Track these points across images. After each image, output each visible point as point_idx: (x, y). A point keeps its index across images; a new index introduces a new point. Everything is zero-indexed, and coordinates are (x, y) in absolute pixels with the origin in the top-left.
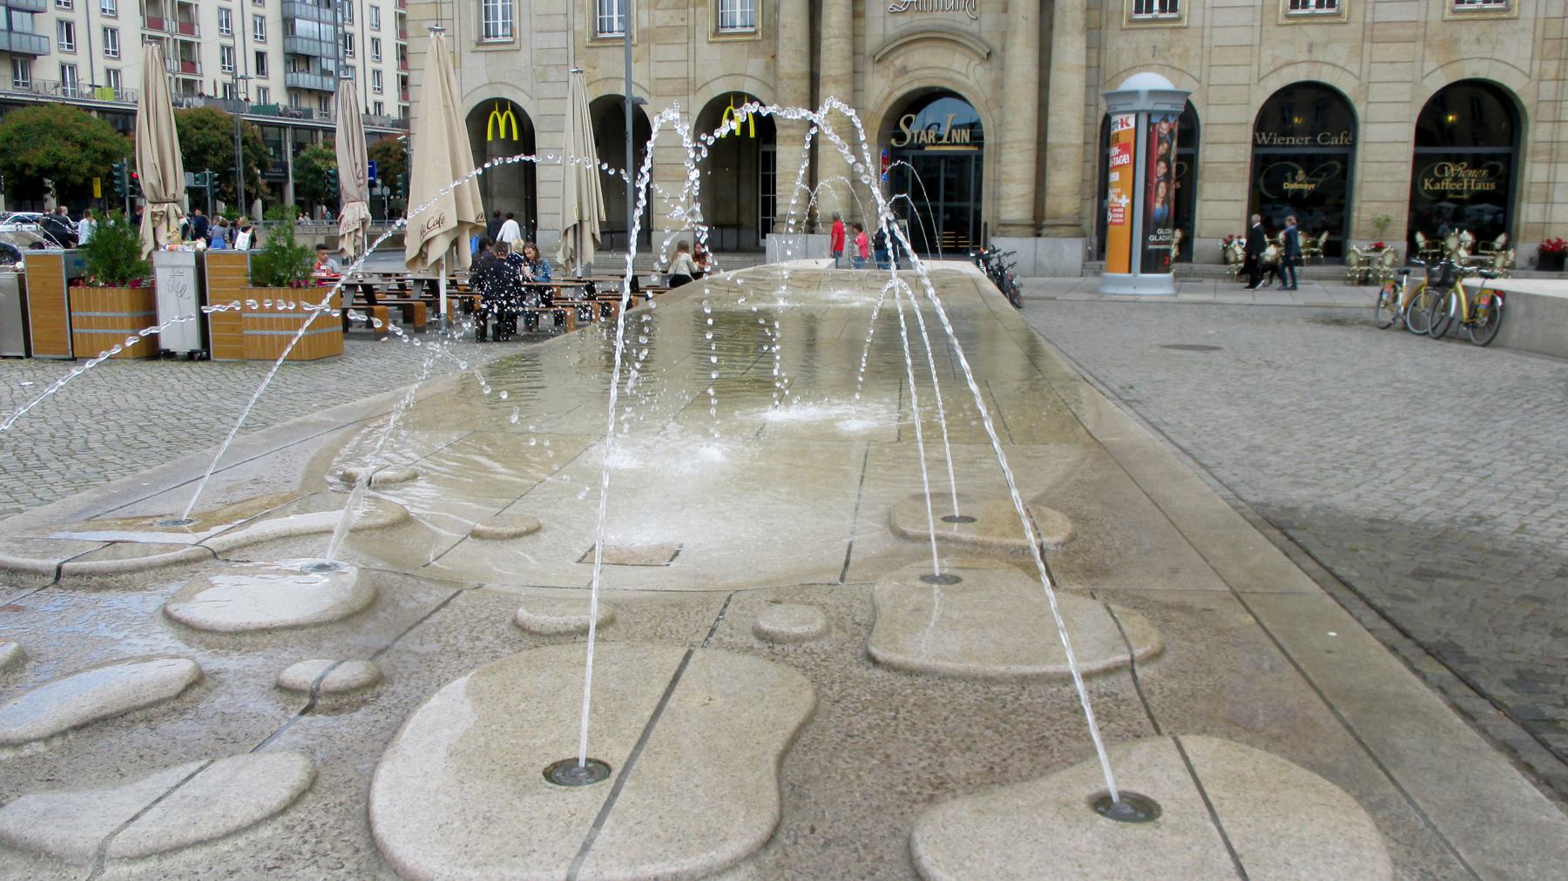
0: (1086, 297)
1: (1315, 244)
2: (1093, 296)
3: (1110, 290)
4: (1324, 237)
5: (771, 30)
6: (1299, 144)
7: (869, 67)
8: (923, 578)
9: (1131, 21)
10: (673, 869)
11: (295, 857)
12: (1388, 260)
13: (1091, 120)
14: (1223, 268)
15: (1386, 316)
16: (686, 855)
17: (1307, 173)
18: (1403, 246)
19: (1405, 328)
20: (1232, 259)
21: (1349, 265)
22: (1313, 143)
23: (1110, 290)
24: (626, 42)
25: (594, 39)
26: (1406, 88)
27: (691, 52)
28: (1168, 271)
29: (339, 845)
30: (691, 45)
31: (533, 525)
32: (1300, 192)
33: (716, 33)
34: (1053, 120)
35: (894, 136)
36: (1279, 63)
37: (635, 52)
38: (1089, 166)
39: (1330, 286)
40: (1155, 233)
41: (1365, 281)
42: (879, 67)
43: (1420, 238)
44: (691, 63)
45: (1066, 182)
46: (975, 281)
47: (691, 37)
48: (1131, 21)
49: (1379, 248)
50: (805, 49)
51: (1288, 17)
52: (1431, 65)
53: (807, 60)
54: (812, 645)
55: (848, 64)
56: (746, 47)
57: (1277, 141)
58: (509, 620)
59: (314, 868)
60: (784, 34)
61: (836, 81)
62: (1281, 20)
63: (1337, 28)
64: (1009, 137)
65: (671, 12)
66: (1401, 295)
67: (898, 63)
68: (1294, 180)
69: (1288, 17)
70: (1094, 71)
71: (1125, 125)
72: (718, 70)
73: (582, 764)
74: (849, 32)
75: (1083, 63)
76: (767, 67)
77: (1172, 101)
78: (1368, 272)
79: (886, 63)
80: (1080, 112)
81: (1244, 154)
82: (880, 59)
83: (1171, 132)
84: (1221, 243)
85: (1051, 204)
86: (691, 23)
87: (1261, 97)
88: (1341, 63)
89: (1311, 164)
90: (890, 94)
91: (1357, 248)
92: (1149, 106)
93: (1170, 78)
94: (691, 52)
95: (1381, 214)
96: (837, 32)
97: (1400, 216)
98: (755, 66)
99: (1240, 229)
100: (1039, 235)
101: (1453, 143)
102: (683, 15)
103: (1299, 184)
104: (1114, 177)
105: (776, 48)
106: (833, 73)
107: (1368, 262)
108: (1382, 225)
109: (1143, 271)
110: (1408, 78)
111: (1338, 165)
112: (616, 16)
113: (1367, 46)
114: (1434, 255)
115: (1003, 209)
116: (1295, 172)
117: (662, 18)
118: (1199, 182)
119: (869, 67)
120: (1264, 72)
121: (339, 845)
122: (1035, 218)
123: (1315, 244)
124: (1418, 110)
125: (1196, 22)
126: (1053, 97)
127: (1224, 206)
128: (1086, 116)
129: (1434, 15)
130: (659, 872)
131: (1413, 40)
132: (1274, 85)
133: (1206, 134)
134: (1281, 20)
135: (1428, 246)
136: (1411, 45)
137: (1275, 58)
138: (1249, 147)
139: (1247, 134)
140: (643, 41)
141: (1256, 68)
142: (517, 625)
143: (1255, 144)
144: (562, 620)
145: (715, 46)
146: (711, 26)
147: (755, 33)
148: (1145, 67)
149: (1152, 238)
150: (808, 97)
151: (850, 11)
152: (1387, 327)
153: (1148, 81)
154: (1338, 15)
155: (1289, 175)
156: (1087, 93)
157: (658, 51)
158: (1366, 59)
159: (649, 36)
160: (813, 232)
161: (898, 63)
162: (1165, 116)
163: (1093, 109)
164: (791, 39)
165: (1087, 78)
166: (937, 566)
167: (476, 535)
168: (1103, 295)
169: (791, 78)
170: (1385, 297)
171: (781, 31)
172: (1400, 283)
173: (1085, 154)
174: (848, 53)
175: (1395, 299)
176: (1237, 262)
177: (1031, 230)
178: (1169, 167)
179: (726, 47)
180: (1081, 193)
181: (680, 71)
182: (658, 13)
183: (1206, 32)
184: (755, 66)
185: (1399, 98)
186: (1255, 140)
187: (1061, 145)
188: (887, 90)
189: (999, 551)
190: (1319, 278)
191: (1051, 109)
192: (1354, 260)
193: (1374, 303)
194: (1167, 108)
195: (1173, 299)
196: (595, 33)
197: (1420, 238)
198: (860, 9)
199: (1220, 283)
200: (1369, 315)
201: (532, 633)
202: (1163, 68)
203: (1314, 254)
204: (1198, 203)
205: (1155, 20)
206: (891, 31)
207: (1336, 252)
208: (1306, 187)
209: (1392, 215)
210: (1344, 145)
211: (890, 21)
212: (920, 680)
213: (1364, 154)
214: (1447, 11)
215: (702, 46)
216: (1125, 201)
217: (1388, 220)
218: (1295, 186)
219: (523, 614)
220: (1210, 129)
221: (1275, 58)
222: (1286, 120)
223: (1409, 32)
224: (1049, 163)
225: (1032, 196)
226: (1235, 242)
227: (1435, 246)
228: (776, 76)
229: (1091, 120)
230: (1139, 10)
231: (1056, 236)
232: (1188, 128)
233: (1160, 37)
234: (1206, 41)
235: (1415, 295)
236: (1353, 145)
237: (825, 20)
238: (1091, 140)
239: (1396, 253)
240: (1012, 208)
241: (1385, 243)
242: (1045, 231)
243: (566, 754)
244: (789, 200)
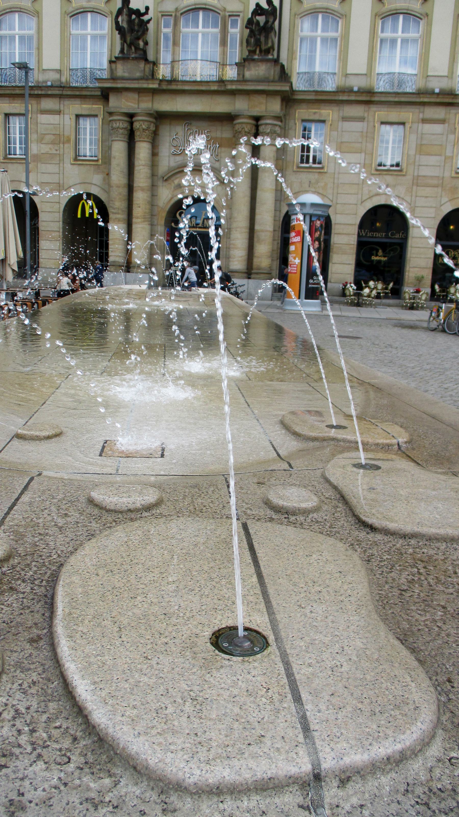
0: (277, 311)
1: (386, 288)
2: (280, 311)
3: (288, 308)
4: (391, 285)
5: (106, 159)
6: (380, 237)
7: (160, 183)
8: (355, 466)
9: (298, 167)
10: (399, 747)
11: (17, 751)
12: (424, 298)
13: (277, 219)
14: (342, 299)
15: (434, 324)
16: (398, 729)
17: (384, 251)
18: (429, 290)
19: (444, 331)
20: (348, 294)
21: (405, 299)
22: (387, 237)
23: (288, 308)
24: (25, 161)
25: (5, 158)
26: (433, 210)
27: (62, 168)
28: (317, 299)
29: (56, 733)
30: (61, 165)
31: (57, 431)
32: (379, 262)
33: (76, 159)
34: (258, 217)
35: (173, 221)
36: (371, 194)
37: (31, 166)
38: (276, 243)
39: (395, 310)
40: (312, 279)
41: (412, 308)
42: (165, 184)
43: (437, 287)
44: (61, 176)
45: (265, 250)
46: (229, 298)
47: (61, 160)
48: (298, 167)
49: (418, 291)
50: (126, 170)
51: (377, 170)
52: (445, 199)
53: (127, 177)
54: (315, 515)
55: (149, 181)
56: (92, 168)
57: (369, 234)
58: (83, 499)
59: (41, 765)
60: (114, 163)
61: (143, 189)
62: (373, 172)
63: (400, 178)
64: (234, 225)
65: (50, 146)
66: (442, 314)
67: (176, 182)
68: (377, 255)
69: (377, 170)
70: (279, 193)
71: (299, 221)
72: (77, 181)
73: (241, 633)
74: (150, 163)
75: (274, 188)
76: (104, 180)
77: (323, 210)
78: (413, 303)
79: (170, 181)
80: (272, 214)
81: (354, 240)
82: (167, 179)
83: (321, 225)
84: (341, 286)
85: (256, 261)
86: (61, 153)
87: (362, 211)
88: (402, 196)
89: (384, 246)
90: (172, 198)
91: (408, 290)
92: (311, 211)
93: (323, 199)
94: (62, 168)
95: (419, 274)
96: (143, 163)
97: (428, 275)
98: (97, 179)
99: (351, 278)
100: (249, 278)
101: (454, 240)
102: (57, 148)
103: (379, 257)
104: (292, 248)
105: (109, 169)
106: (141, 185)
107: (414, 298)
108: (420, 280)
109: (306, 298)
110: (434, 205)
111: (398, 248)
112: (18, 146)
113: (415, 188)
114: (443, 296)
115: (231, 263)
116: (377, 251)
117: (45, 148)
118: (331, 254)
119: (160, 183)
120: (364, 198)
121: (56, 733)
122: (247, 269)
123: (386, 288)
124: (438, 222)
125: (331, 170)
126: (258, 205)
127: (343, 266)
128: (275, 216)
129: (447, 174)
130: (389, 751)
131: (437, 186)
132: (369, 205)
133: (335, 229)
134: (373, 172)
135: (440, 291)
136: (436, 189)
137: (370, 191)
138: (356, 237)
139: (355, 230)
140: (34, 161)
141: (360, 196)
142: (91, 501)
143: (359, 236)
144: (131, 500)
145: (75, 167)
146: (72, 155)
147: (97, 161)
148: (306, 192)
149: (311, 281)
150: (126, 197)
151: (150, 152)
152: (434, 330)
153: (311, 198)
154: (401, 171)
155: (374, 252)
156: (275, 204)
157: (43, 167)
158: (414, 193)
159: (37, 158)
160: (129, 272)
161: (176, 182)
162: (319, 217)
163: (278, 213)
164: (118, 165)
165: (276, 196)
166: (362, 457)
167: (18, 436)
168: (285, 310)
169: (118, 187)
170: (433, 314)
171: (112, 160)
172: (441, 308)
173: (274, 236)
174: (149, 175)
175: (438, 316)
176: (350, 296)
177: (246, 275)
178: (320, 244)
179: (82, 167)
180: (271, 257)
181: (55, 179)
182: (43, 146)
183: (336, 176)
184: (97, 179)
185: (429, 216)
186: (358, 233)
187: (262, 231)
188: (170, 196)
189: (373, 447)
190: (389, 305)
191: (257, 211)
192: (407, 296)
193: (427, 318)
194: (320, 213)
195: (321, 313)
196: (6, 155)
197: (437, 287)
198: (156, 151)
199: (342, 307)
200: (425, 325)
201: (108, 511)
202: (318, 193)
203: (386, 293)
204: (330, 265)
205: (310, 168)
206: (173, 164)
207: (396, 293)
208: (383, 259)
209: (425, 275)
210: (402, 239)
211: (172, 158)
212: (413, 542)
213: (411, 243)
214: (453, 172)
215: (68, 166)
216: (297, 261)
217: (423, 277)
218: (377, 258)
219: (95, 495)
220: (337, 226)
221: (370, 191)
222: (373, 224)
223: (435, 182)
224: (255, 239)
225: (246, 257)
226: (349, 285)
227: (443, 291)
228: (110, 186)
229: (277, 219)
230: (302, 162)
231: (259, 279)
232: (328, 224)
233: (313, 177)
234: (336, 181)
235: (448, 314)
236: (406, 238)
237: (137, 156)
238: (277, 229)
239: (427, 294)
240: (236, 263)
241: (421, 289)
242: (253, 276)
243: (230, 623)
244: (116, 253)
